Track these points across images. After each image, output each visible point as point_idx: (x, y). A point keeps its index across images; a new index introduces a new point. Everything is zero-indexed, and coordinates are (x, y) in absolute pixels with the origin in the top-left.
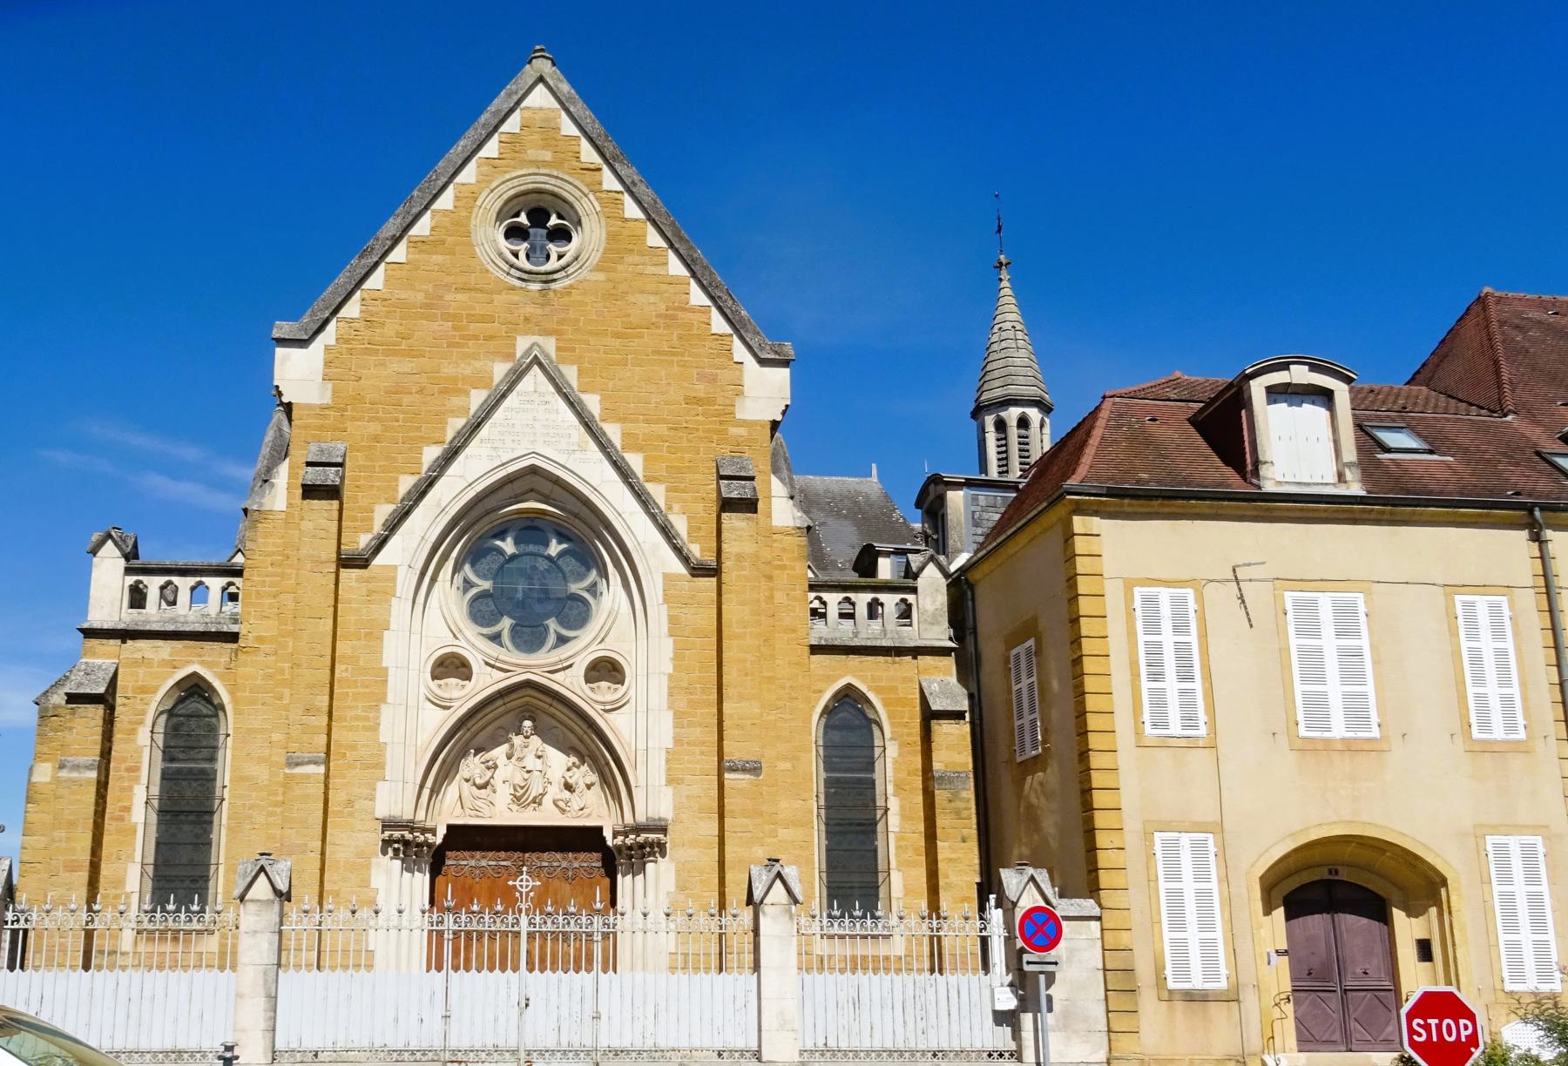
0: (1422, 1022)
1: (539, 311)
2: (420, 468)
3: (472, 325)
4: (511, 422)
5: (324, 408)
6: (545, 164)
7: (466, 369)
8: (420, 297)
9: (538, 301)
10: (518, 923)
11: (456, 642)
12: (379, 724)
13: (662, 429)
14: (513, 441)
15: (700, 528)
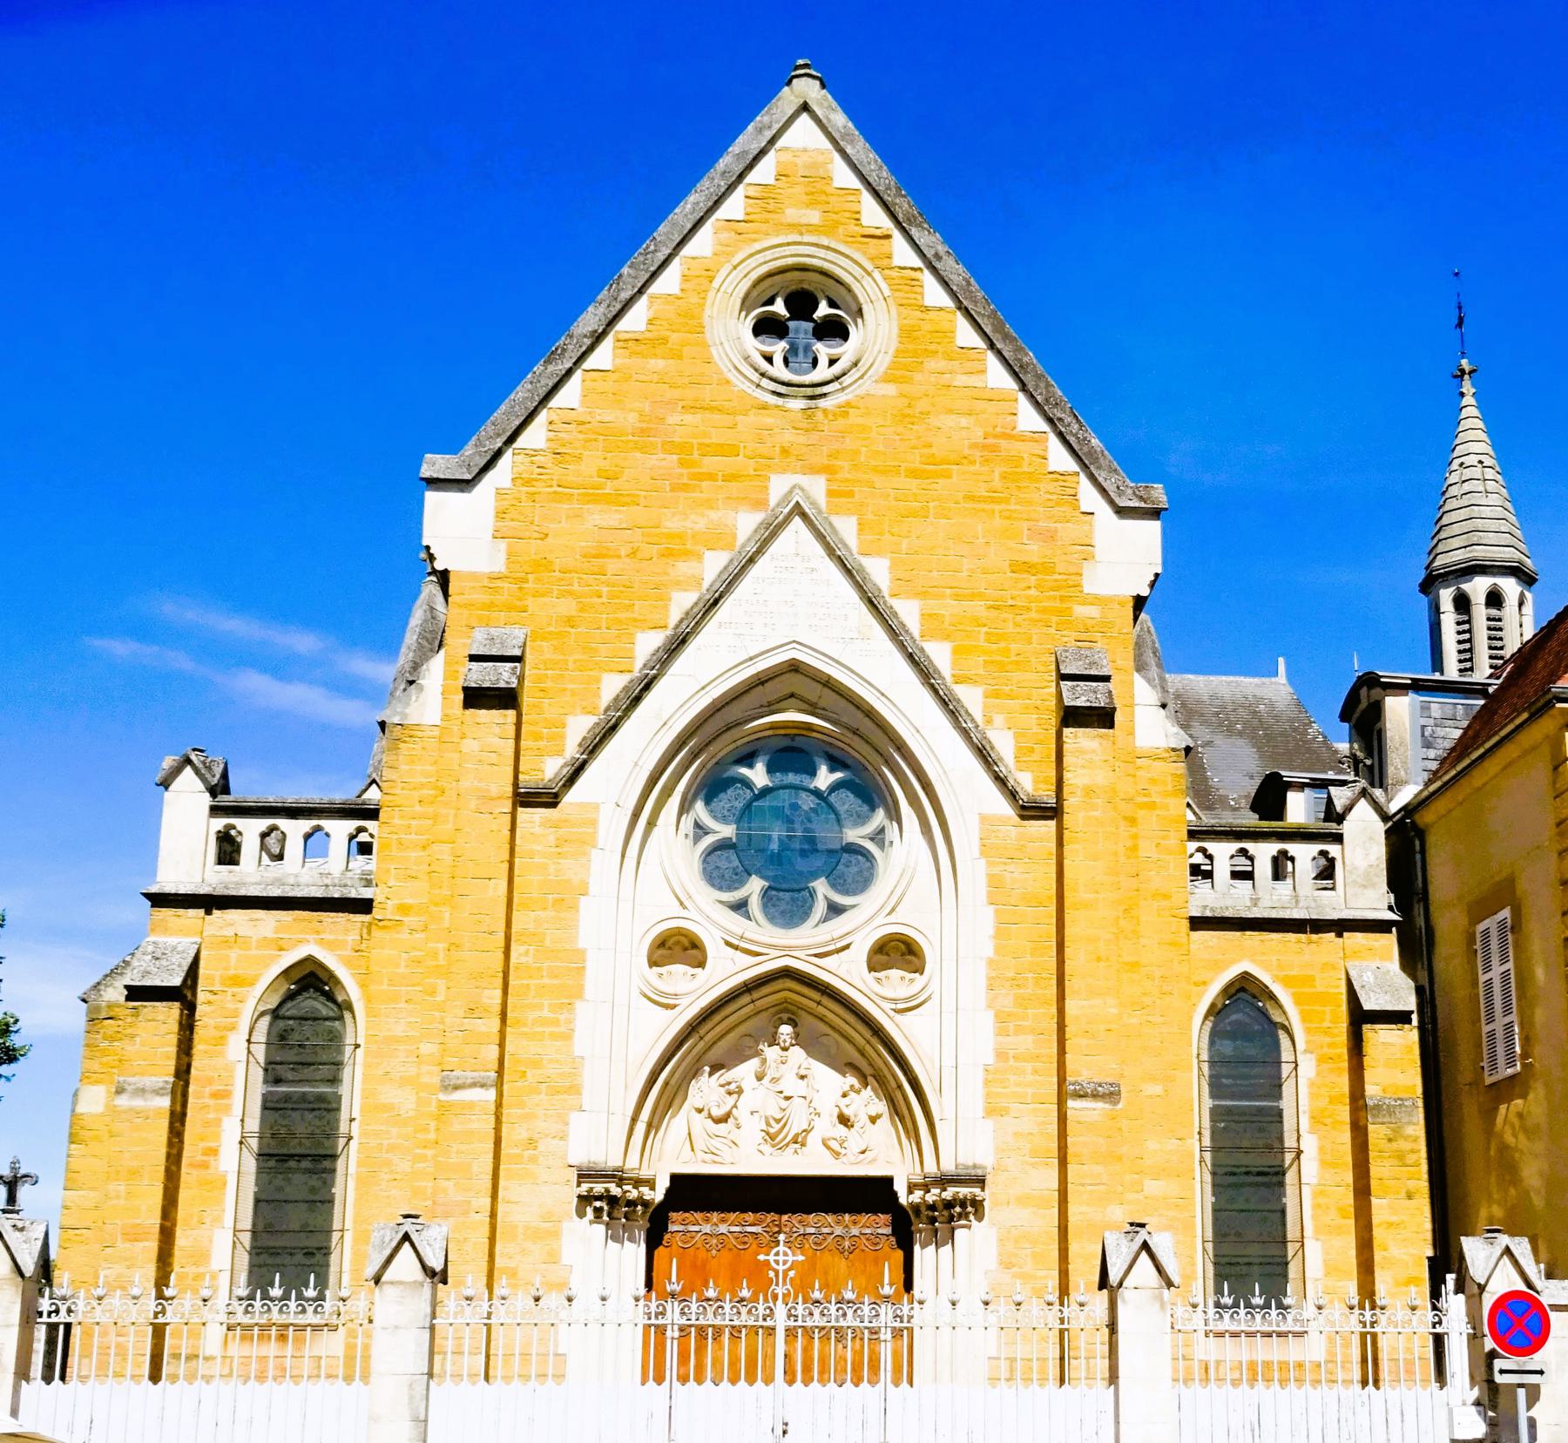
1: (802, 439)
3: (707, 460)
5: (494, 578)
7: (698, 522)
8: (632, 418)
9: (800, 425)
11: (684, 913)
13: (978, 608)
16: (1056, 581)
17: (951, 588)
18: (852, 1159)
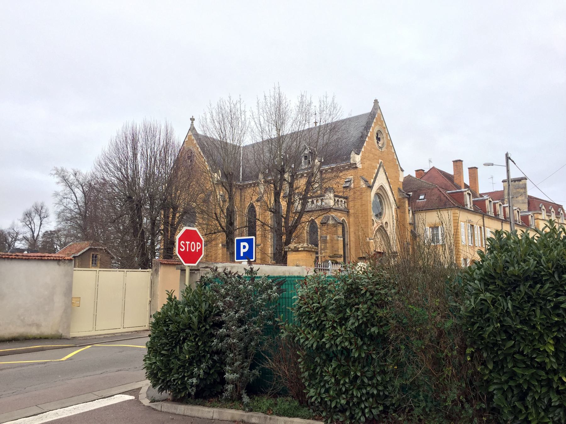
0: (184, 243)
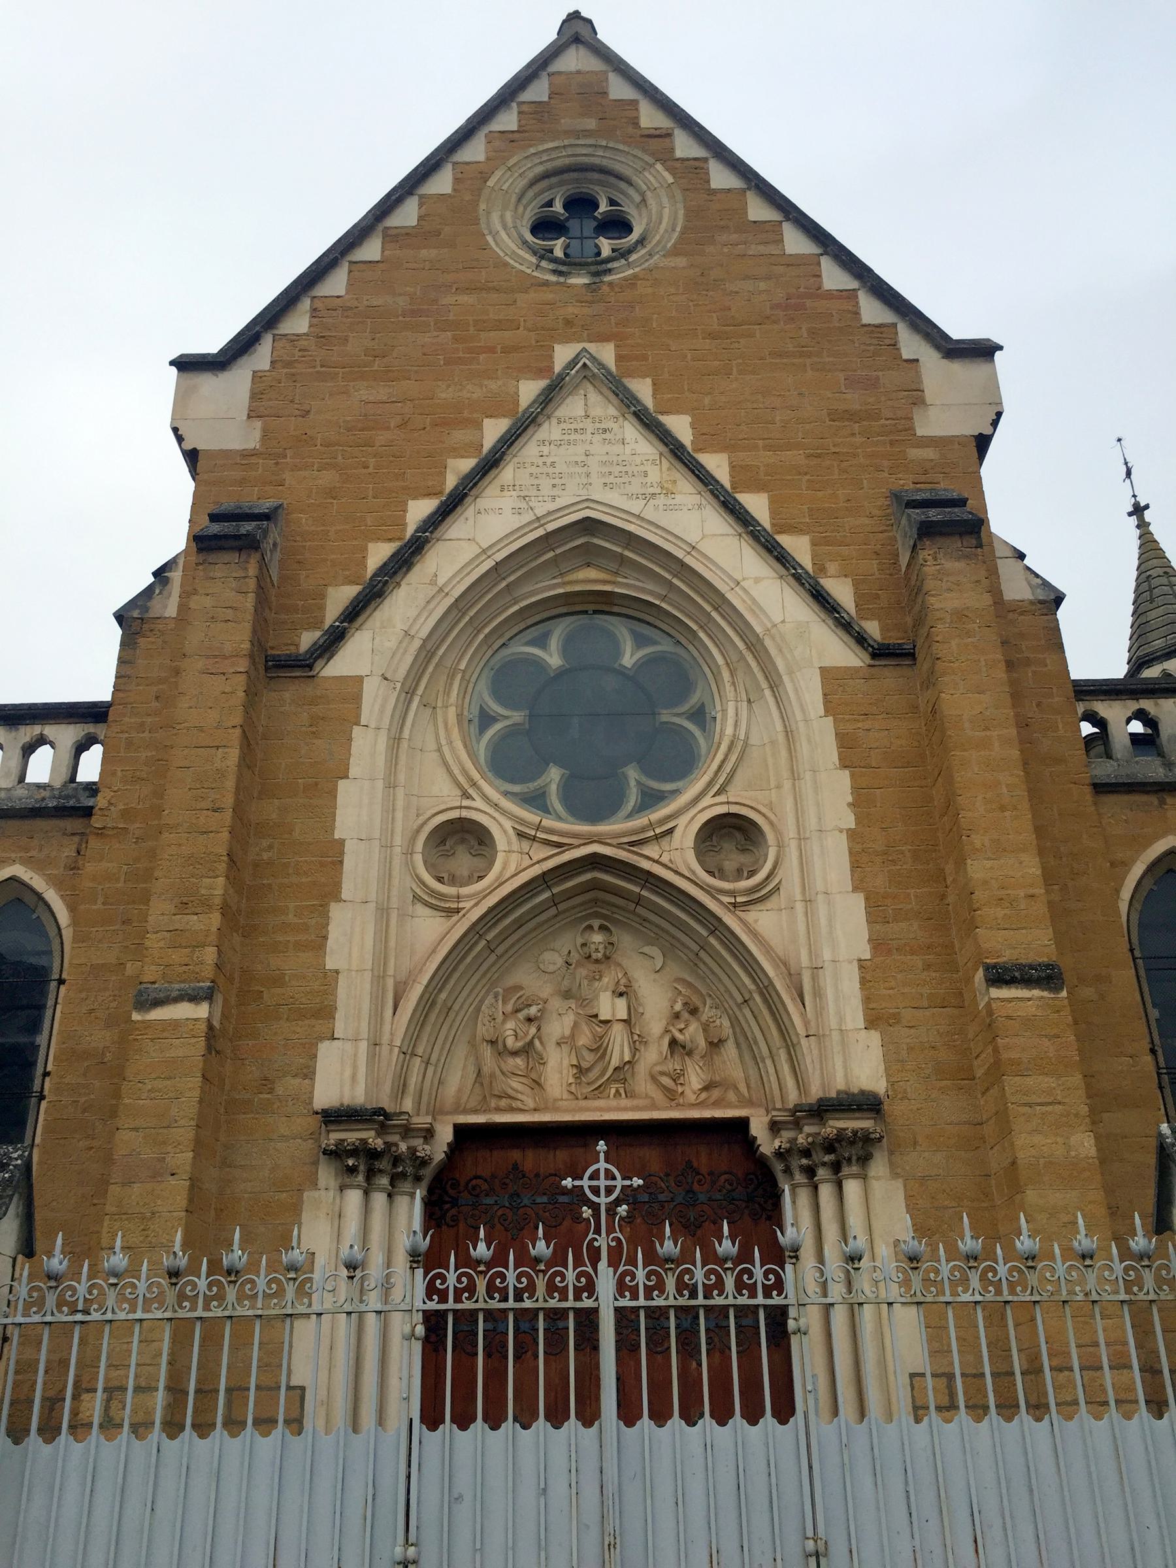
1: (587, 311)
2: (405, 530)
3: (483, 335)
4: (549, 460)
5: (246, 454)
6: (587, 133)
7: (474, 392)
8: (402, 302)
9: (585, 298)
10: (590, 1288)
11: (466, 803)
12: (325, 938)
13: (794, 457)
14: (554, 486)
15: (877, 597)
16: (883, 426)
17: (764, 439)
18: (691, 1098)
